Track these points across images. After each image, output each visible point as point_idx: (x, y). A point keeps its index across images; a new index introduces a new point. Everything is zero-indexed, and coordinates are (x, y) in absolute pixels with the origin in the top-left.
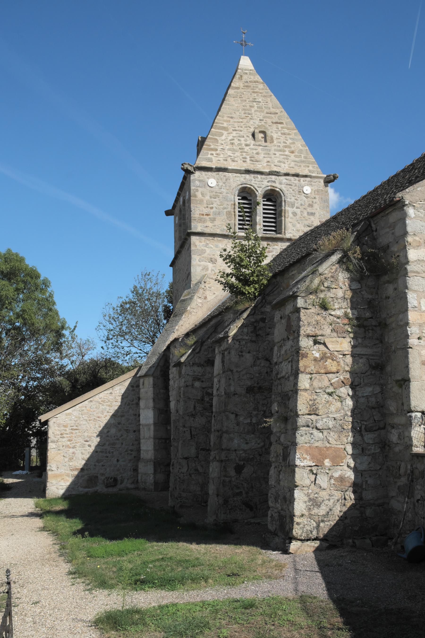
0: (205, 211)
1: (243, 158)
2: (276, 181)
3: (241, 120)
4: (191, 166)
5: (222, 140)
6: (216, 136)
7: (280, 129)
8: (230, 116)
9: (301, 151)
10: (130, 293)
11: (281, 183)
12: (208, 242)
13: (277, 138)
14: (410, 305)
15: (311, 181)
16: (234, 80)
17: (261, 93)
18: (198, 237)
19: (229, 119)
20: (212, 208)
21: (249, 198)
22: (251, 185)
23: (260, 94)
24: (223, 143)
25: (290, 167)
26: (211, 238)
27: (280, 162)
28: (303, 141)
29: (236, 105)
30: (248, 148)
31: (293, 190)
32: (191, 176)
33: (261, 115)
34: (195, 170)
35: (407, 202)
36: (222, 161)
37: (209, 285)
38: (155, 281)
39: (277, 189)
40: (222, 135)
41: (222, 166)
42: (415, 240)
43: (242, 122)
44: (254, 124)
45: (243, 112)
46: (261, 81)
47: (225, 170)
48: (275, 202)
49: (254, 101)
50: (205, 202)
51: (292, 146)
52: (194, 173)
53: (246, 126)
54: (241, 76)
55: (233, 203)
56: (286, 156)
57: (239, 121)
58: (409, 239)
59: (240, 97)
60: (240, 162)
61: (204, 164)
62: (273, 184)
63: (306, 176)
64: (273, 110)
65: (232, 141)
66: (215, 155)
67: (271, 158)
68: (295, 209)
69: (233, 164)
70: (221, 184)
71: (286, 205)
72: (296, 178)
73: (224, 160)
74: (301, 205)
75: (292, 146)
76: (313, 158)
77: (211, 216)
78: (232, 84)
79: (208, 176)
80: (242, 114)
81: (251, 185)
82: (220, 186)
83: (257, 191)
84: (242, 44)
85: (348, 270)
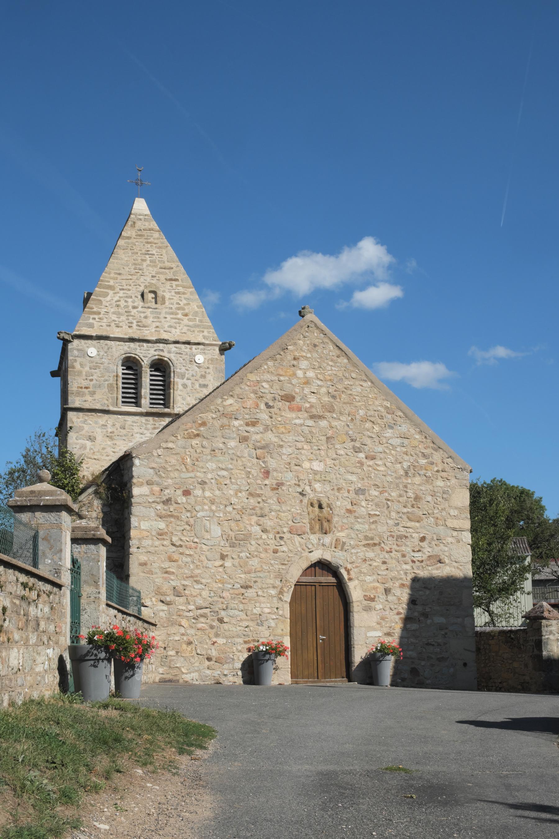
0: (84, 383)
1: (129, 323)
2: (165, 350)
3: (130, 277)
4: (68, 334)
5: (107, 302)
6: (100, 296)
7: (174, 286)
8: (118, 272)
9: (196, 314)
10: (22, 457)
11: (169, 352)
12: (86, 418)
13: (170, 299)
14: (132, 526)
15: (204, 349)
16: (126, 227)
17: (155, 244)
18: (75, 413)
19: (116, 276)
20: (91, 380)
21: (134, 368)
22: (136, 355)
23: (154, 245)
24: (108, 305)
25: (182, 333)
26: (90, 414)
27: (170, 327)
28: (200, 301)
29: (126, 259)
30: (135, 310)
31: (184, 360)
32: (69, 344)
33: (153, 270)
34: (73, 338)
35: (134, 455)
36: (105, 327)
37: (87, 466)
38: (53, 443)
39: (166, 359)
40: (106, 295)
41: (104, 334)
42: (138, 482)
43: (131, 279)
44: (145, 281)
45: (134, 266)
46: (158, 228)
47: (107, 338)
48: (164, 372)
49: (147, 253)
50: (84, 373)
51: (186, 307)
52: (72, 342)
53: (135, 284)
54: (134, 223)
55: (115, 374)
56: (179, 319)
57: (128, 278)
58: (134, 480)
59: (131, 249)
60: (125, 327)
61: (85, 331)
62: (161, 353)
63: (198, 344)
64: (167, 264)
65: (118, 303)
66: (97, 320)
67: (160, 322)
68: (185, 380)
69: (117, 331)
70: (102, 353)
71: (176, 376)
72: (186, 345)
73: (107, 326)
74: (193, 376)
75: (186, 307)
76: (209, 321)
77: (91, 389)
78: (123, 233)
79: (87, 345)
80: (132, 270)
81: (136, 355)
82: (101, 356)
83: (143, 361)
84: (137, 184)
85: (100, 498)
